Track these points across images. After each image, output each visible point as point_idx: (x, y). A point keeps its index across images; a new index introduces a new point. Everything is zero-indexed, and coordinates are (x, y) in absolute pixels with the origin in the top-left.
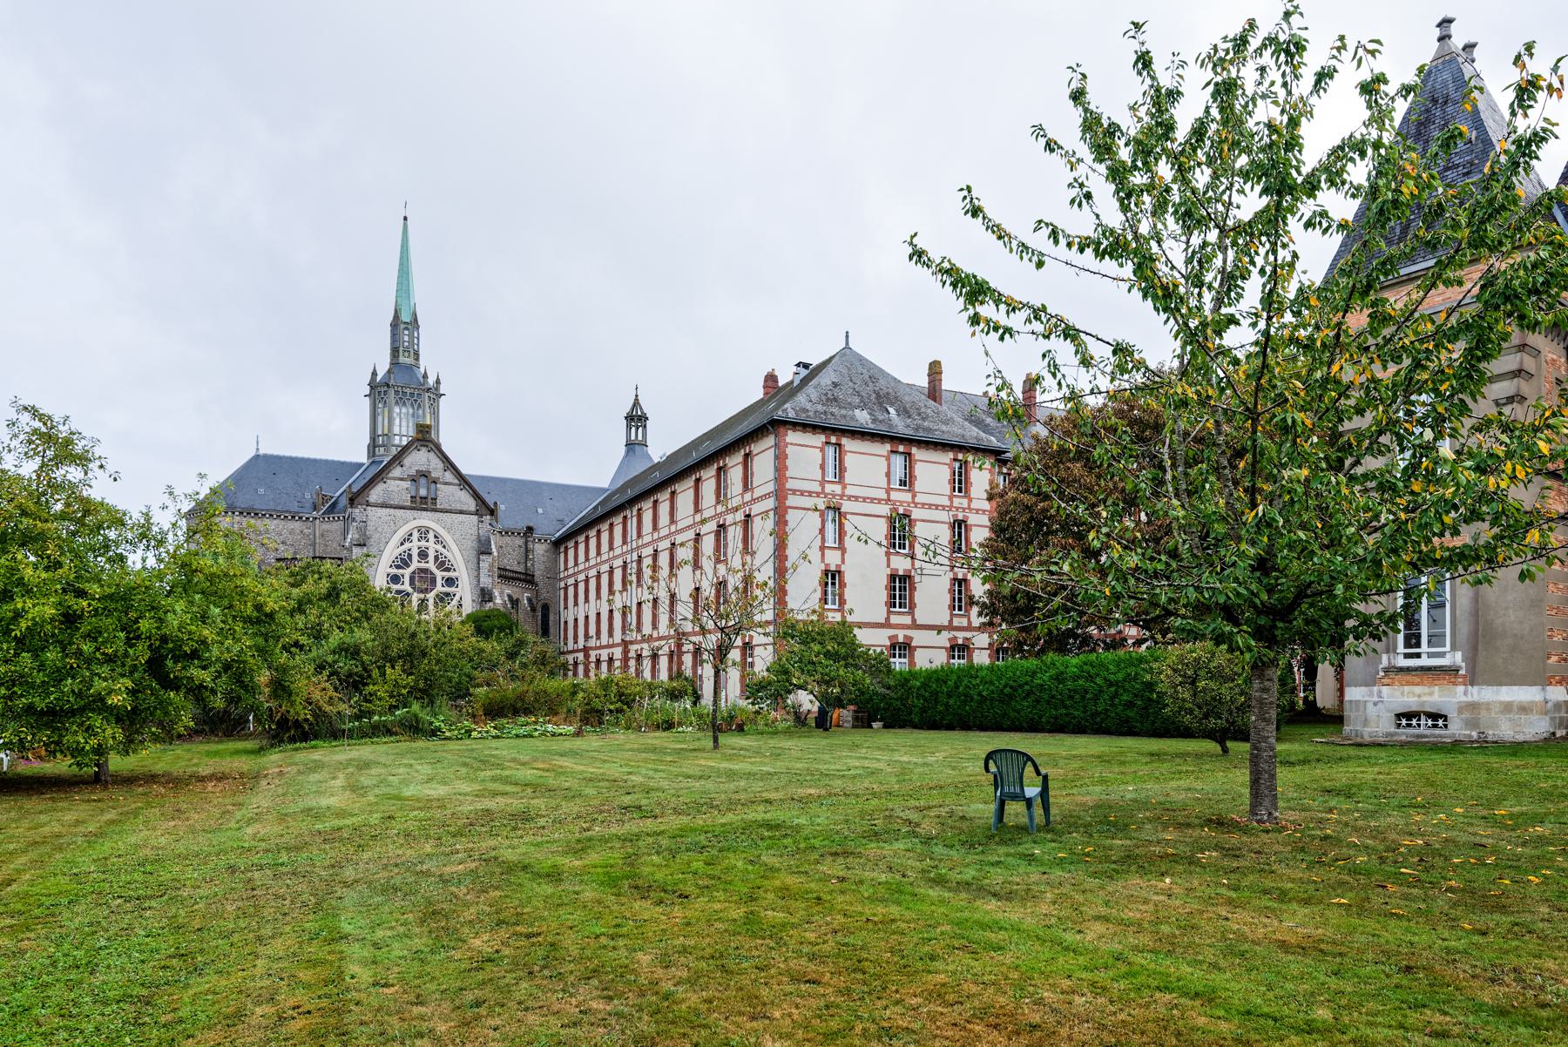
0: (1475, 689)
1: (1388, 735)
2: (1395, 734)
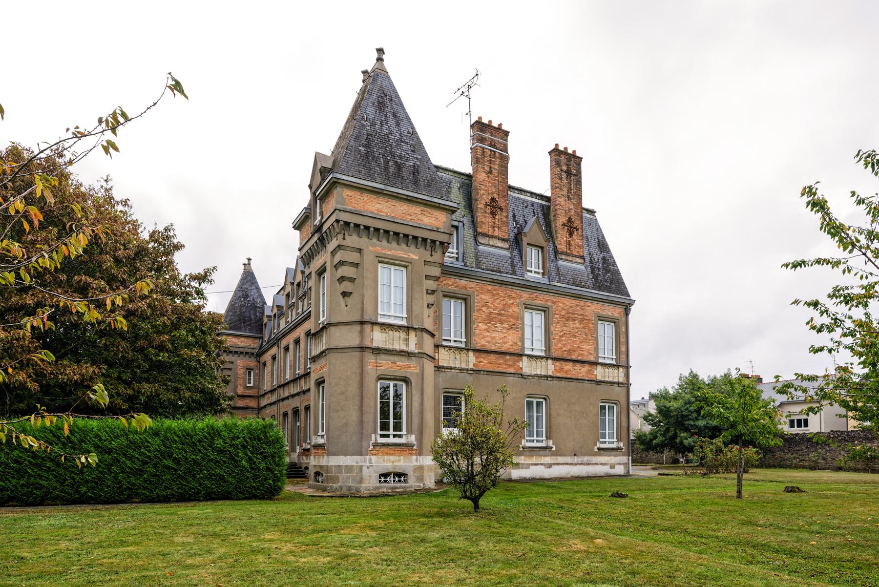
0: (420, 458)
1: (376, 488)
2: (381, 487)
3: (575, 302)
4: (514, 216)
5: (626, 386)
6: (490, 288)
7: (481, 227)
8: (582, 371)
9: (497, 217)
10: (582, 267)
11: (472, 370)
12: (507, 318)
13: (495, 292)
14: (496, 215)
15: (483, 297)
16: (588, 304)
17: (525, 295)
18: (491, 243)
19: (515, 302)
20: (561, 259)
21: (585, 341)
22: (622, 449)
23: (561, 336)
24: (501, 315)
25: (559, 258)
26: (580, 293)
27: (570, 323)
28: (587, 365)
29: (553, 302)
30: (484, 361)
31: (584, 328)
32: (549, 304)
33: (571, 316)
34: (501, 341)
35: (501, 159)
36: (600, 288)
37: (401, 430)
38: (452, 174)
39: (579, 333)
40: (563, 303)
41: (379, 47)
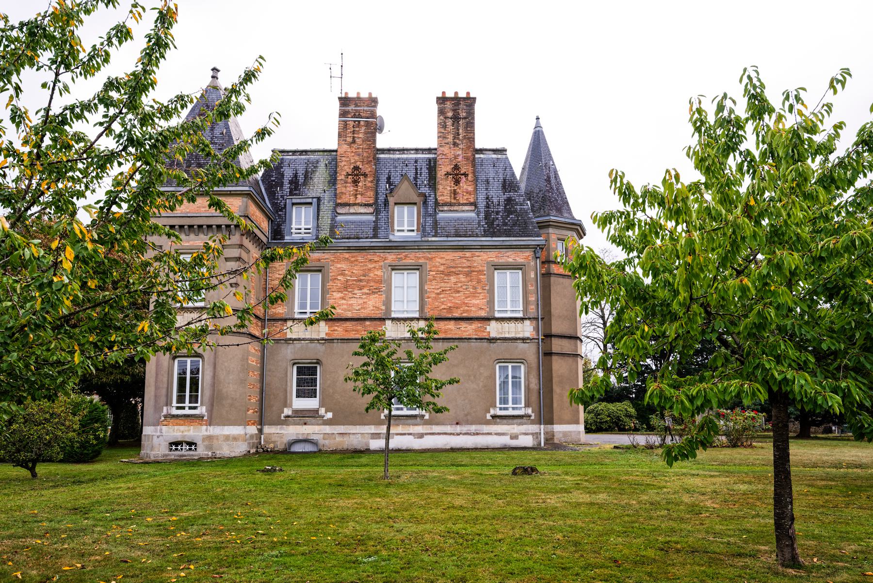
0: (211, 428)
3: (459, 254)
4: (389, 178)
5: (536, 341)
6: (347, 255)
7: (341, 198)
8: (468, 329)
9: (360, 184)
10: (473, 215)
11: (323, 339)
12: (367, 283)
13: (353, 259)
14: (359, 182)
15: (339, 266)
16: (477, 254)
17: (391, 257)
18: (352, 211)
19: (377, 265)
20: (442, 211)
21: (474, 295)
22: (530, 416)
23: (438, 294)
24: (361, 281)
25: (439, 211)
26: (460, 244)
27: (452, 278)
28: (476, 322)
29: (428, 259)
30: (339, 329)
31: (471, 281)
32: (421, 261)
33: (453, 270)
34: (360, 307)
35: (366, 126)
36: (493, 235)
37: (197, 402)
38: (321, 153)
39: (464, 287)
40: (442, 258)
41: (212, 67)
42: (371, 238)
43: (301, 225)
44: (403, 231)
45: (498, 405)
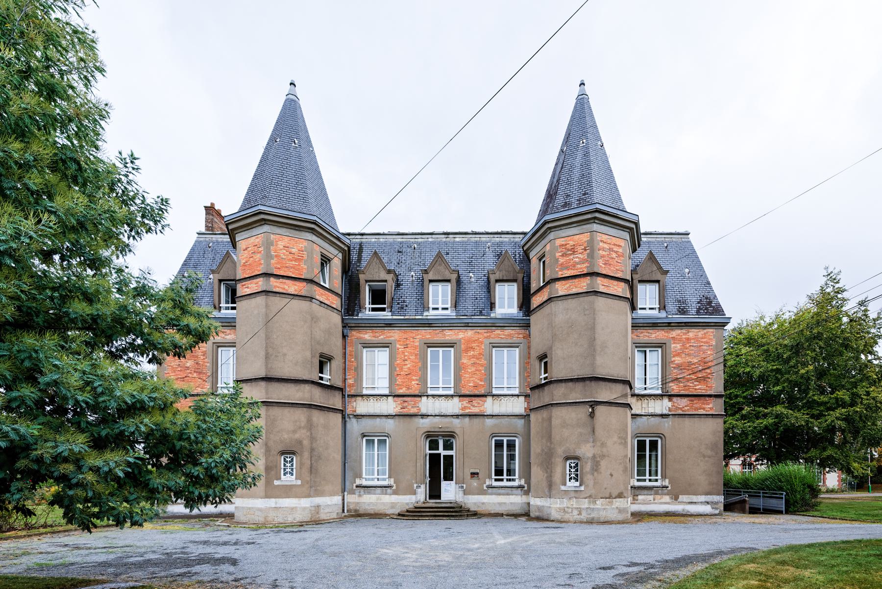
42: (477, 315)
43: (438, 304)
44: (437, 309)
45: (364, 476)
